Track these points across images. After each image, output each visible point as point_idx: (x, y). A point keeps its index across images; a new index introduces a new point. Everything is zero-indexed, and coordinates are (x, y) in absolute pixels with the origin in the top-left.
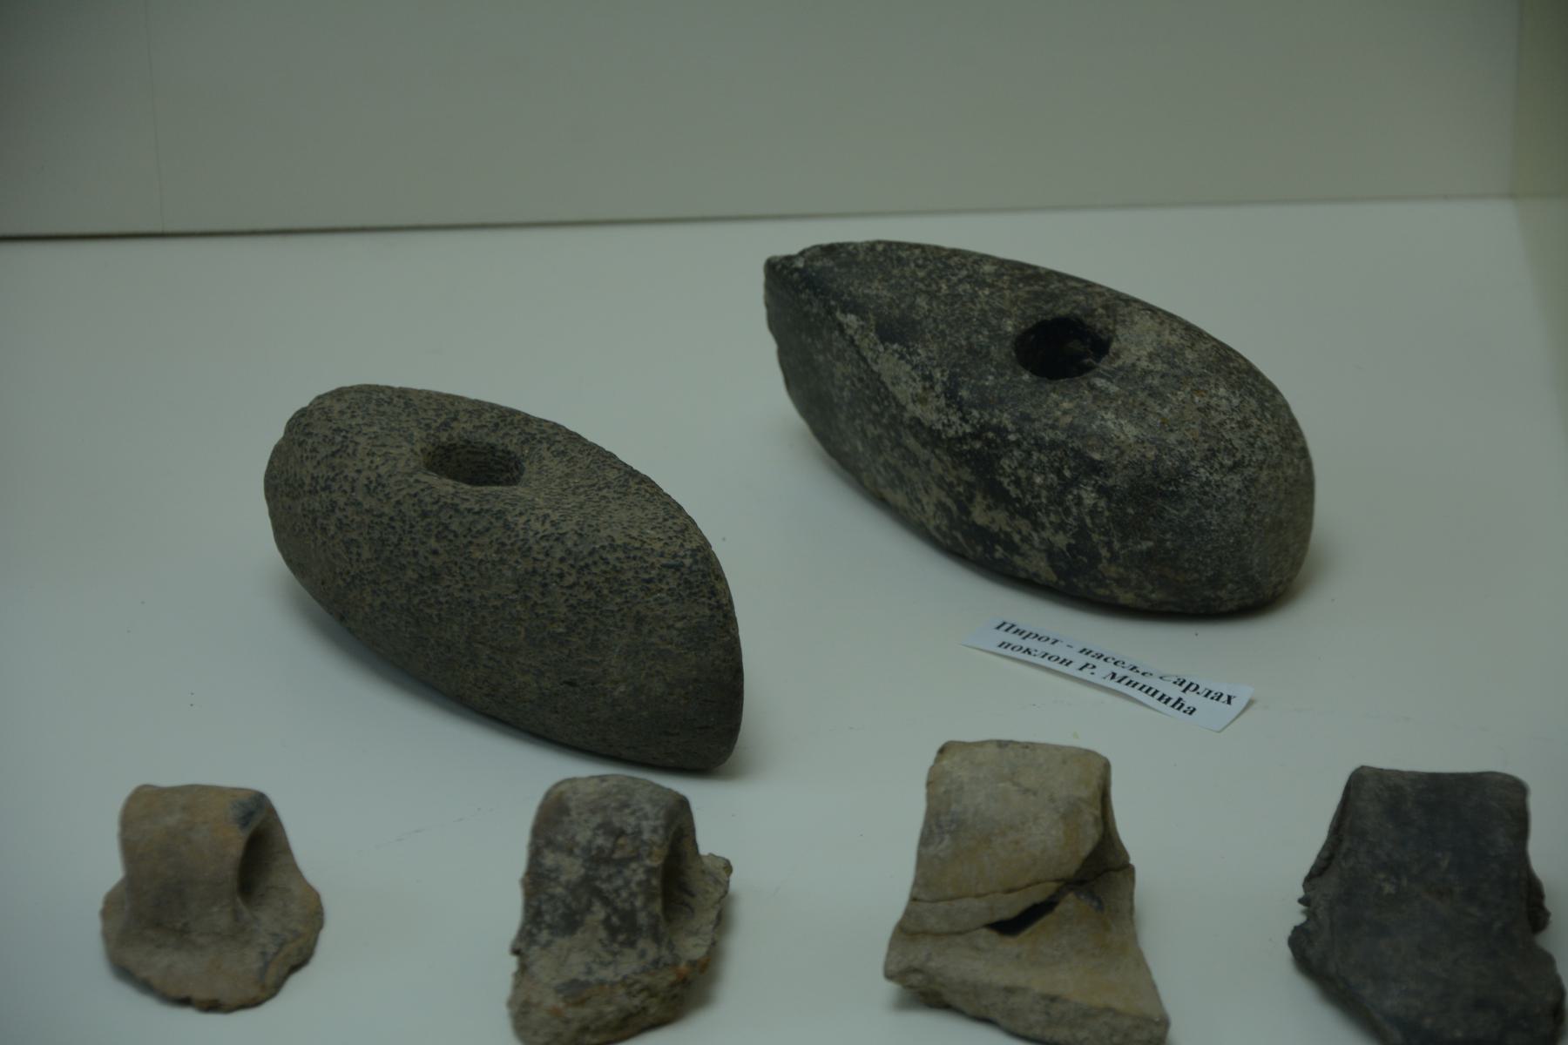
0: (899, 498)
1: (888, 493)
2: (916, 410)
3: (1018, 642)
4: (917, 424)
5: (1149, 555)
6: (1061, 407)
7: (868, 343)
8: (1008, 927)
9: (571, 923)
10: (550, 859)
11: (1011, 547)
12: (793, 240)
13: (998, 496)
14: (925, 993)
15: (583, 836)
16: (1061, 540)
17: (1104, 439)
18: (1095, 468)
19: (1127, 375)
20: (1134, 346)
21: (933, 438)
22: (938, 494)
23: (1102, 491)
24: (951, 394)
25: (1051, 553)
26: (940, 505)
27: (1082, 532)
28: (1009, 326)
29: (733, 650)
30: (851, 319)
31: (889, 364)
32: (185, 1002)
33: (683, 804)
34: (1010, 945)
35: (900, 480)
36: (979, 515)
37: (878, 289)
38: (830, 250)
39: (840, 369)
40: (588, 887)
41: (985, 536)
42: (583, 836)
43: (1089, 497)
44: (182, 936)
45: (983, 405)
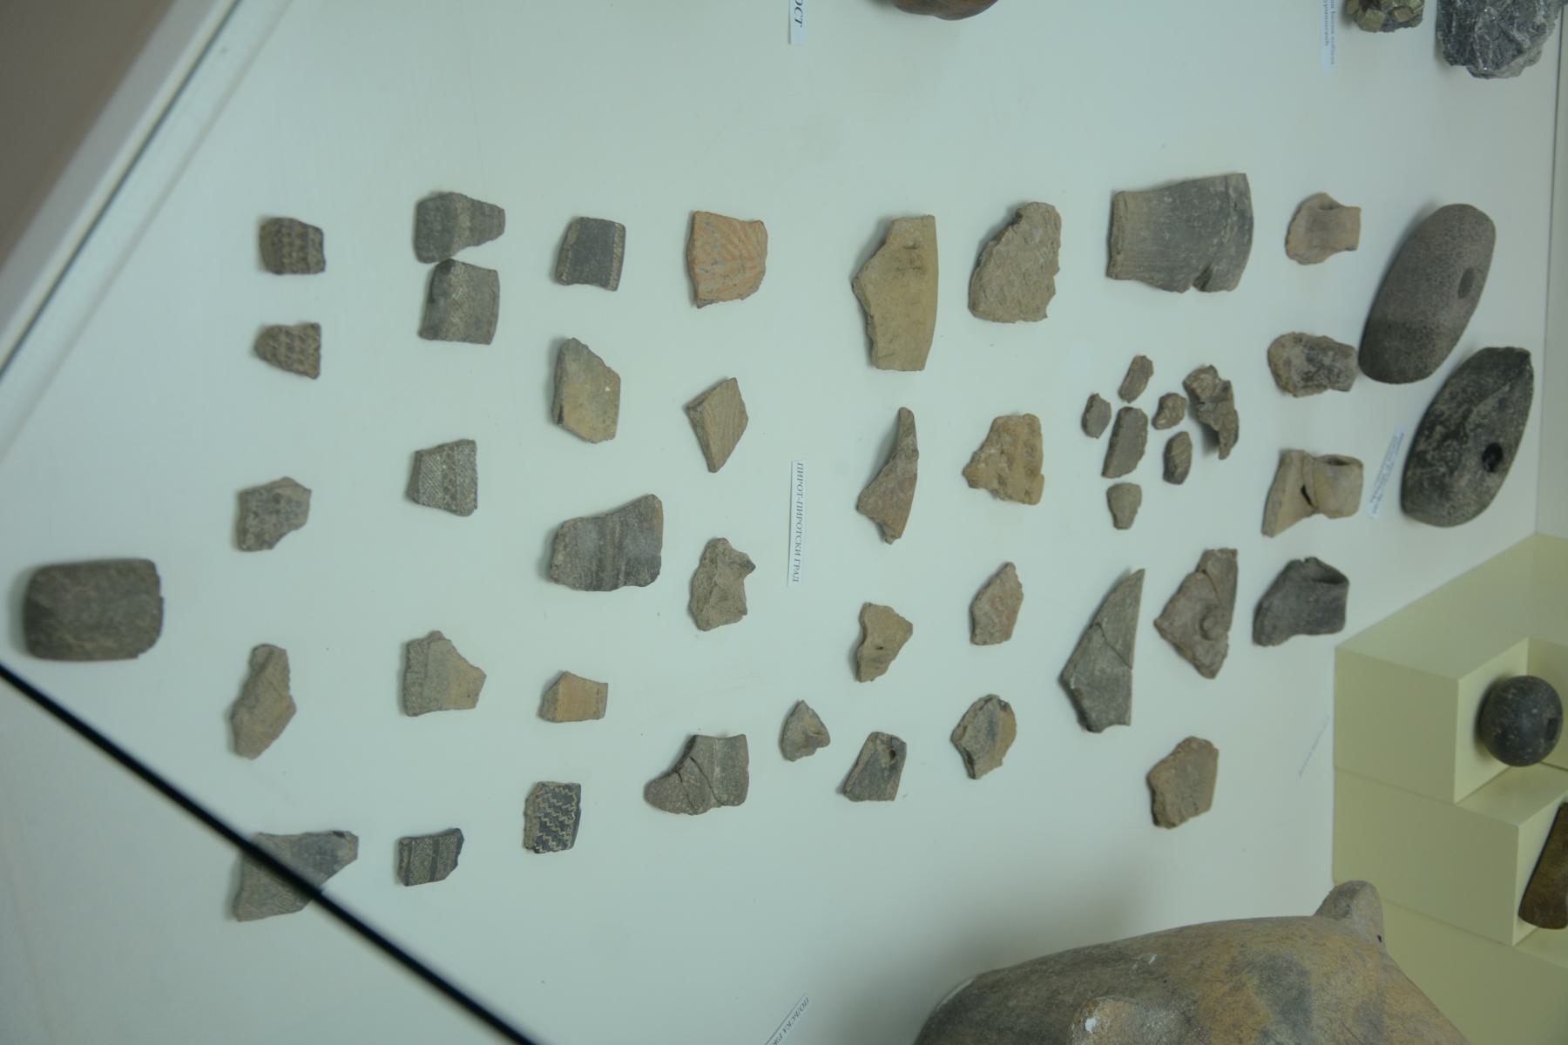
0: (1446, 395)
1: (1448, 391)
2: (1475, 411)
3: (1396, 442)
4: (1470, 411)
5: (1422, 485)
6: (1472, 461)
7: (1499, 394)
8: (1303, 490)
9: (1310, 360)
10: (1331, 353)
11: (1428, 437)
12: (1536, 363)
13: (1445, 437)
14: (1285, 459)
15: (1338, 365)
16: (1429, 457)
17: (1461, 476)
18: (1452, 472)
19: (1482, 480)
20: (1491, 480)
21: (1465, 417)
22: (1447, 413)
23: (1444, 475)
24: (1479, 425)
25: (1425, 452)
26: (1442, 414)
27: (1431, 465)
28: (1501, 440)
29: (1397, 382)
30: (1507, 388)
31: (1491, 402)
32: (1289, 232)
33: (1413, 20)
34: (1298, 491)
35: (1453, 398)
36: (1439, 428)
37: (1517, 394)
38: (1531, 377)
39: (1491, 380)
40: (1321, 366)
41: (1432, 429)
42: (1338, 365)
43: (1443, 470)
44: (1310, 230)
45: (1476, 436)
